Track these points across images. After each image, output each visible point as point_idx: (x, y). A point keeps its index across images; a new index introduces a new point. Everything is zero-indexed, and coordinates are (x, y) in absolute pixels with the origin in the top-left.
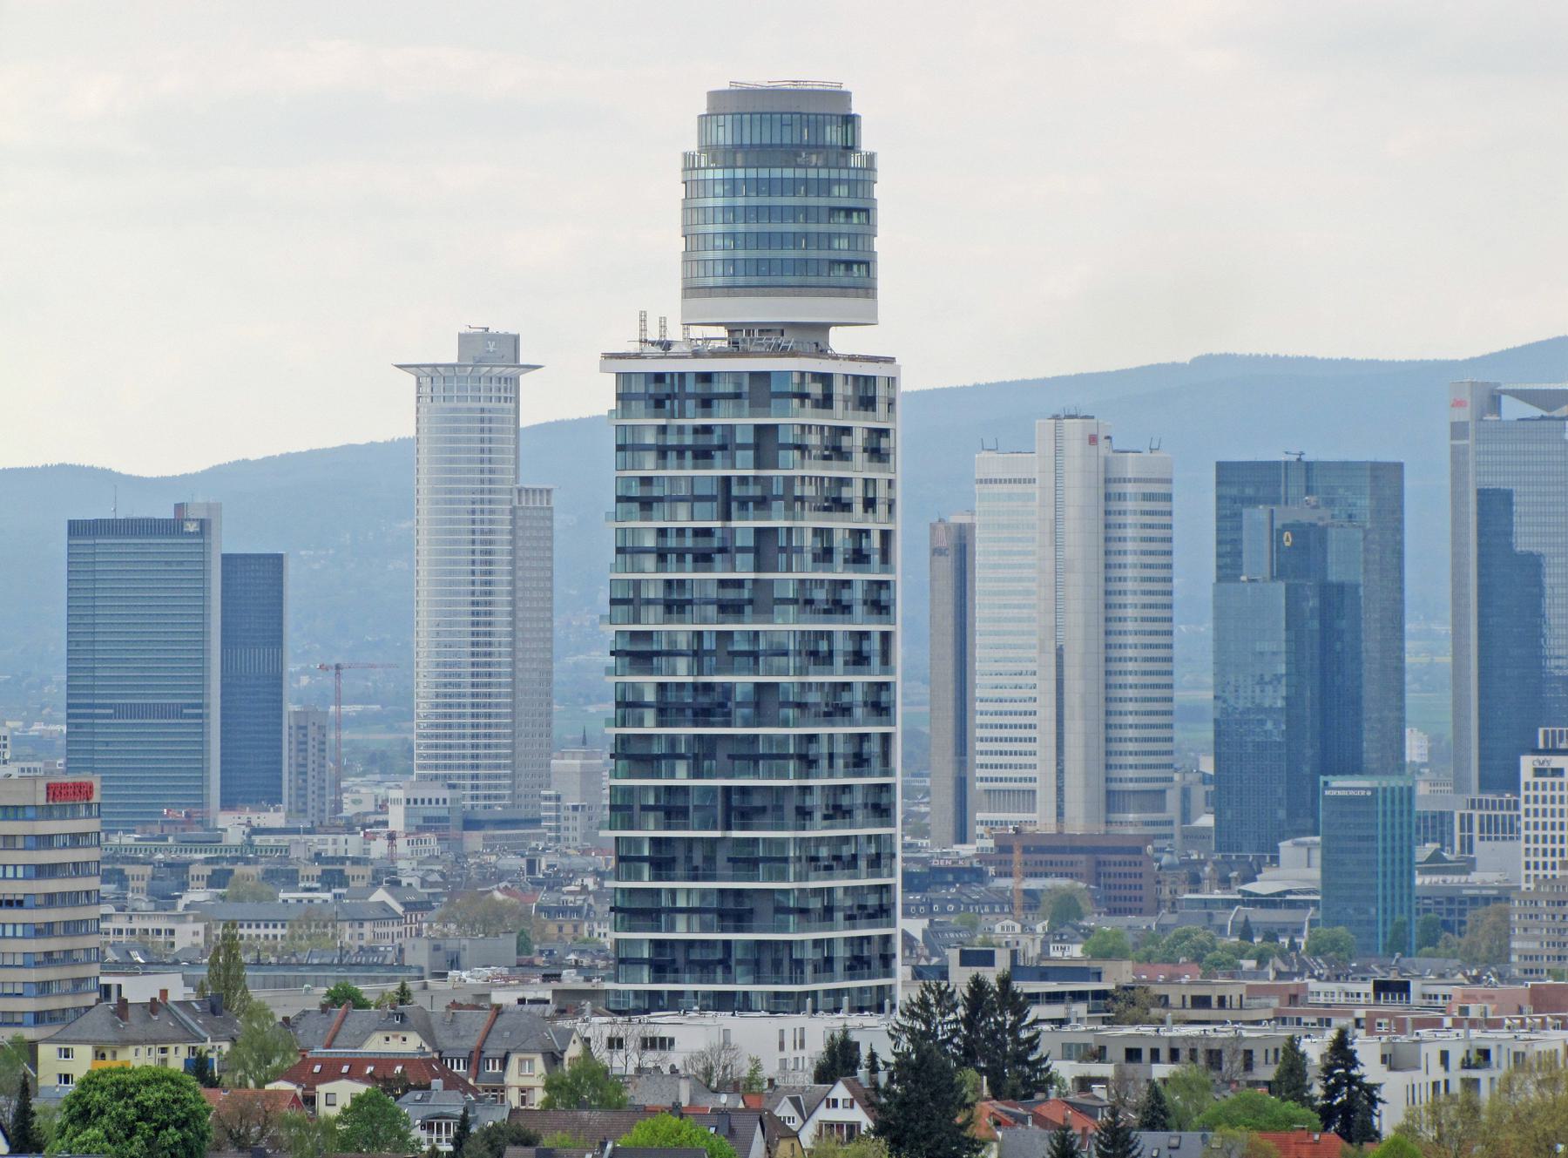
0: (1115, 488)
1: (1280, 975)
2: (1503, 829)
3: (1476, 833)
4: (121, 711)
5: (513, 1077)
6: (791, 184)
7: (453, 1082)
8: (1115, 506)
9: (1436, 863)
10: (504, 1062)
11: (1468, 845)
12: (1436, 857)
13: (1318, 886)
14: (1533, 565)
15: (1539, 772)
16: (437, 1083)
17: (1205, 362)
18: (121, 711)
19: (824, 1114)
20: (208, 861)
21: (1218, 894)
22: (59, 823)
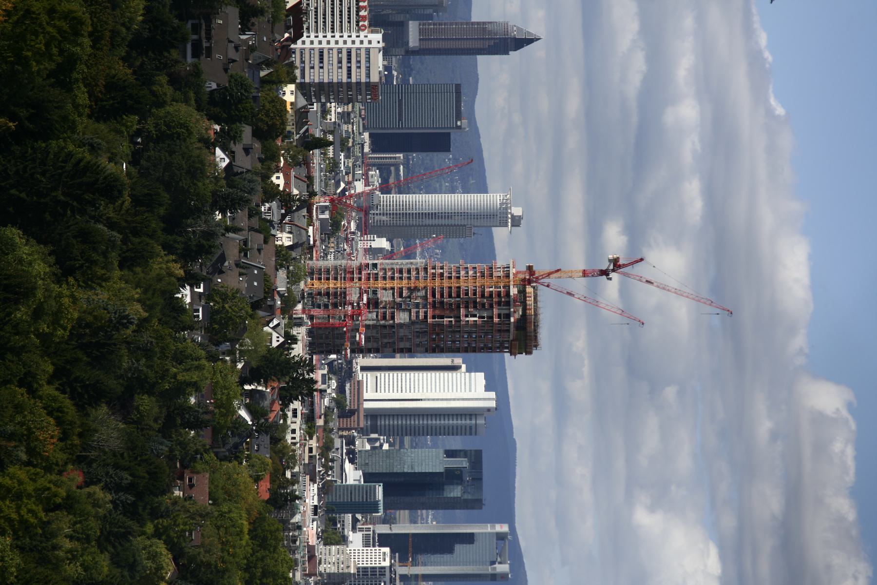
0: (473, 418)
1: (320, 472)
2: (366, 544)
3: (365, 533)
4: (400, 101)
5: (285, 235)
6: (507, 42)
7: (283, 216)
8: (468, 417)
9: (355, 521)
10: (290, 232)
11: (361, 530)
12: (358, 520)
13: (348, 483)
14: (450, 551)
15: (384, 554)
16: (283, 211)
17: (514, 442)
18: (400, 101)
19: (275, 335)
20: (353, 130)
21: (345, 451)
22: (423, 568)
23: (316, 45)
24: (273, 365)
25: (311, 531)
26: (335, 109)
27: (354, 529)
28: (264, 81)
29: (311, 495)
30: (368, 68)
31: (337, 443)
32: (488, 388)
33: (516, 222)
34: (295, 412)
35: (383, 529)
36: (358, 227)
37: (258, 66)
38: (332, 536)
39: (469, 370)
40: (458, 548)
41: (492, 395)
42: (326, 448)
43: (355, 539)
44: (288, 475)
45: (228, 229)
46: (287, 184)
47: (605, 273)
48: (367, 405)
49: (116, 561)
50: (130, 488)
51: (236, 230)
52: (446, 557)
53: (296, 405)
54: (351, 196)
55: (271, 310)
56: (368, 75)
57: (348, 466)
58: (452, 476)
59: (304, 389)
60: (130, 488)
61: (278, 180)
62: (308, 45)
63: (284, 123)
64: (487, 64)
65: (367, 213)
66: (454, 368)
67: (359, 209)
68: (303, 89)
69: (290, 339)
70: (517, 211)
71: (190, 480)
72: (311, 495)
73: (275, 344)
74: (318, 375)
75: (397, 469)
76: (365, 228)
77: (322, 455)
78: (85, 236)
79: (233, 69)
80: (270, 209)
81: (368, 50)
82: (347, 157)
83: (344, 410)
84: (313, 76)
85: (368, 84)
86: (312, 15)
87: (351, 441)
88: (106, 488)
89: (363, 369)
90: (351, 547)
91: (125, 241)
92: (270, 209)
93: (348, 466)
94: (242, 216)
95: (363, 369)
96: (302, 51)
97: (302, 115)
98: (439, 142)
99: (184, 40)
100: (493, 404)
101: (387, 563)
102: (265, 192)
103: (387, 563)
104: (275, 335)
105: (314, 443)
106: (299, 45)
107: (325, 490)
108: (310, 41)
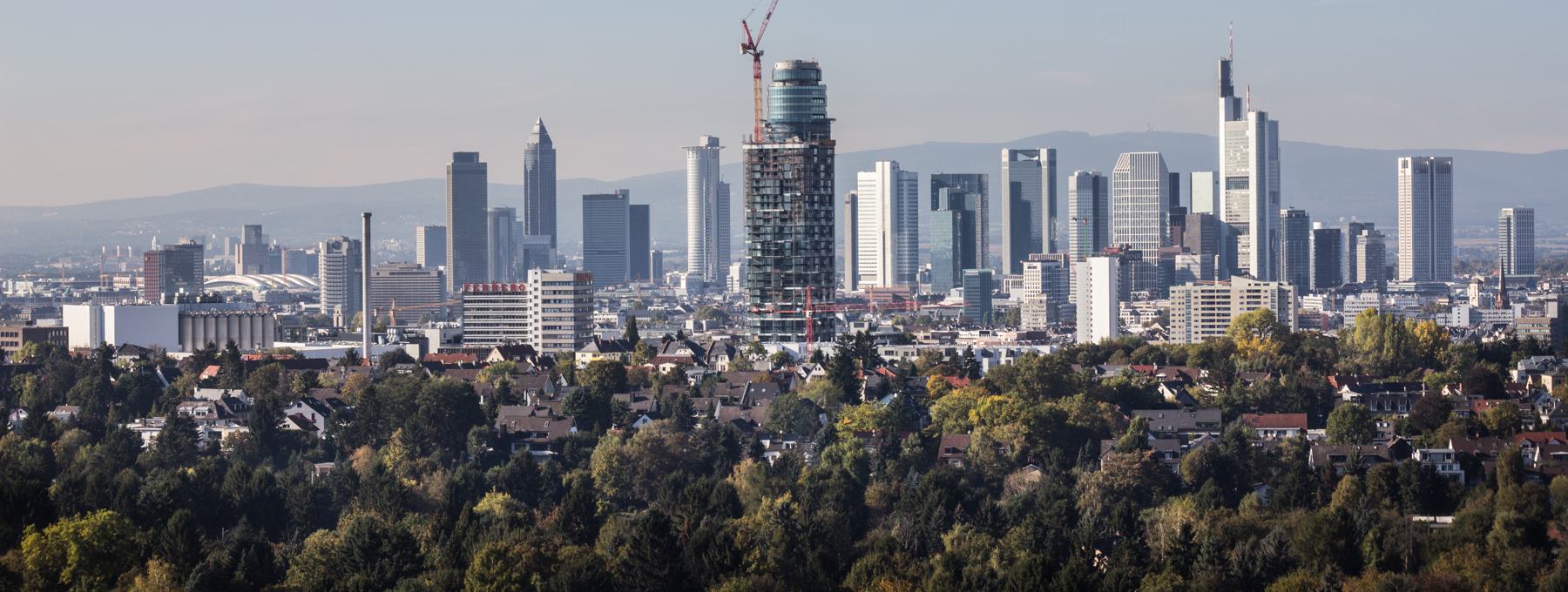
2: (1020, 284)
9: (999, 296)
14: (1027, 205)
23: (540, 332)
24: (844, 376)
25: (1005, 338)
26: (599, 316)
27: (1008, 296)
28: (572, 382)
29: (971, 339)
30: (561, 283)
31: (925, 312)
32: (873, 169)
33: (714, 142)
34: (887, 353)
35: (1006, 269)
36: (720, 293)
37: (558, 388)
38: (1011, 318)
39: (856, 188)
40: (1025, 197)
41: (879, 165)
42: (928, 322)
43: (1016, 295)
44: (947, 359)
45: (711, 416)
46: (670, 360)
47: (757, 57)
48: (889, 284)
49: (1017, 522)
50: (950, 507)
51: (712, 409)
52: (1034, 209)
53: (881, 350)
54: (690, 300)
55: (789, 376)
56: (567, 283)
57: (947, 302)
58: (956, 203)
59: (864, 348)
60: (950, 507)
61: (666, 368)
62: (540, 341)
63: (612, 363)
64: (565, 171)
65: (706, 285)
66: (854, 200)
67: (703, 293)
68: (579, 346)
69: (818, 357)
70: (704, 142)
71: (948, 451)
72: (971, 339)
73: (822, 372)
74: (853, 331)
75: (950, 255)
76: (721, 284)
77: (935, 326)
78: (702, 548)
79: (559, 411)
80: (693, 376)
81: (544, 284)
82: (651, 303)
83: (894, 304)
84: (567, 338)
85: (576, 283)
86: (510, 337)
87: (923, 299)
88: (947, 527)
89: (854, 288)
90: (1025, 300)
91: (712, 513)
92: (693, 376)
93: (947, 302)
94: (697, 403)
95: (854, 288)
96: (544, 346)
97: (605, 346)
98: (641, 215)
99: (529, 456)
100: (888, 164)
101: (1039, 265)
102: (676, 382)
103: (1039, 265)
104: (814, 372)
105: (920, 335)
106: (540, 350)
107: (968, 324)
108: (535, 338)
